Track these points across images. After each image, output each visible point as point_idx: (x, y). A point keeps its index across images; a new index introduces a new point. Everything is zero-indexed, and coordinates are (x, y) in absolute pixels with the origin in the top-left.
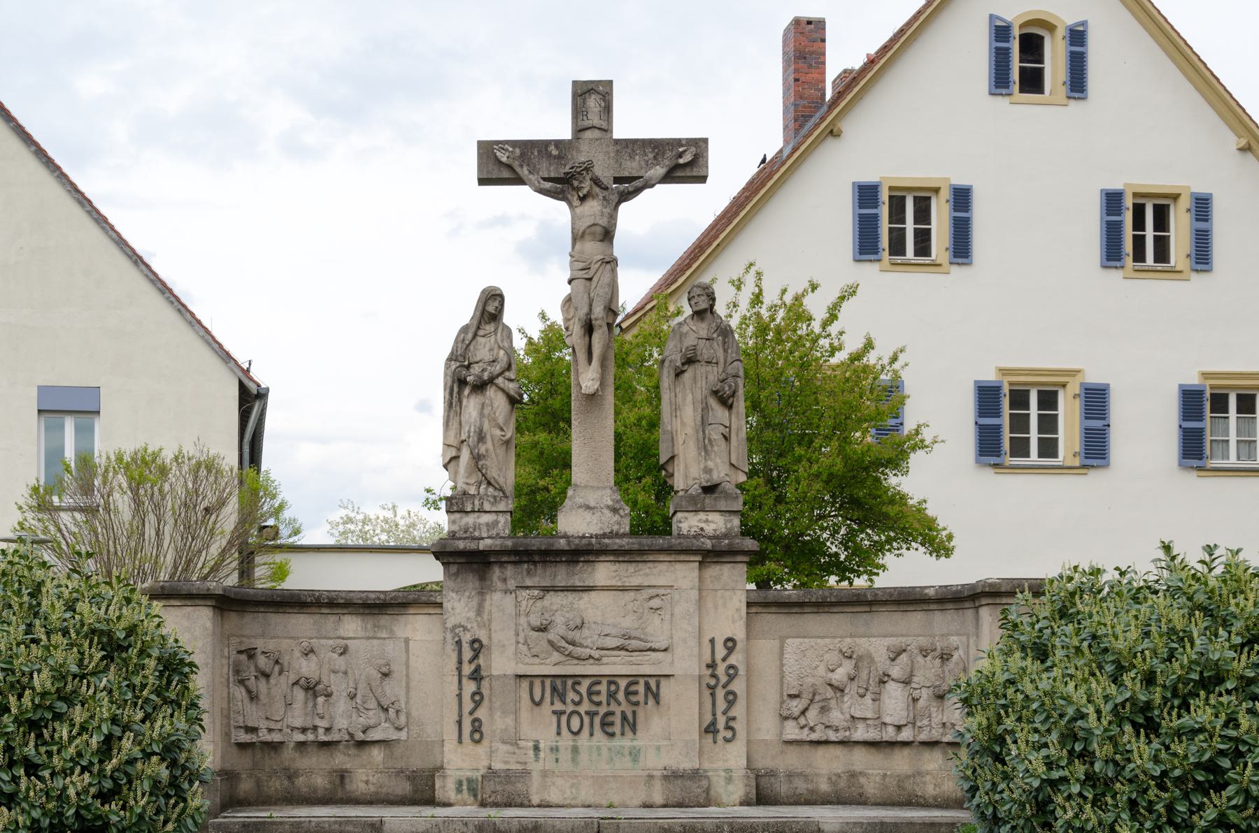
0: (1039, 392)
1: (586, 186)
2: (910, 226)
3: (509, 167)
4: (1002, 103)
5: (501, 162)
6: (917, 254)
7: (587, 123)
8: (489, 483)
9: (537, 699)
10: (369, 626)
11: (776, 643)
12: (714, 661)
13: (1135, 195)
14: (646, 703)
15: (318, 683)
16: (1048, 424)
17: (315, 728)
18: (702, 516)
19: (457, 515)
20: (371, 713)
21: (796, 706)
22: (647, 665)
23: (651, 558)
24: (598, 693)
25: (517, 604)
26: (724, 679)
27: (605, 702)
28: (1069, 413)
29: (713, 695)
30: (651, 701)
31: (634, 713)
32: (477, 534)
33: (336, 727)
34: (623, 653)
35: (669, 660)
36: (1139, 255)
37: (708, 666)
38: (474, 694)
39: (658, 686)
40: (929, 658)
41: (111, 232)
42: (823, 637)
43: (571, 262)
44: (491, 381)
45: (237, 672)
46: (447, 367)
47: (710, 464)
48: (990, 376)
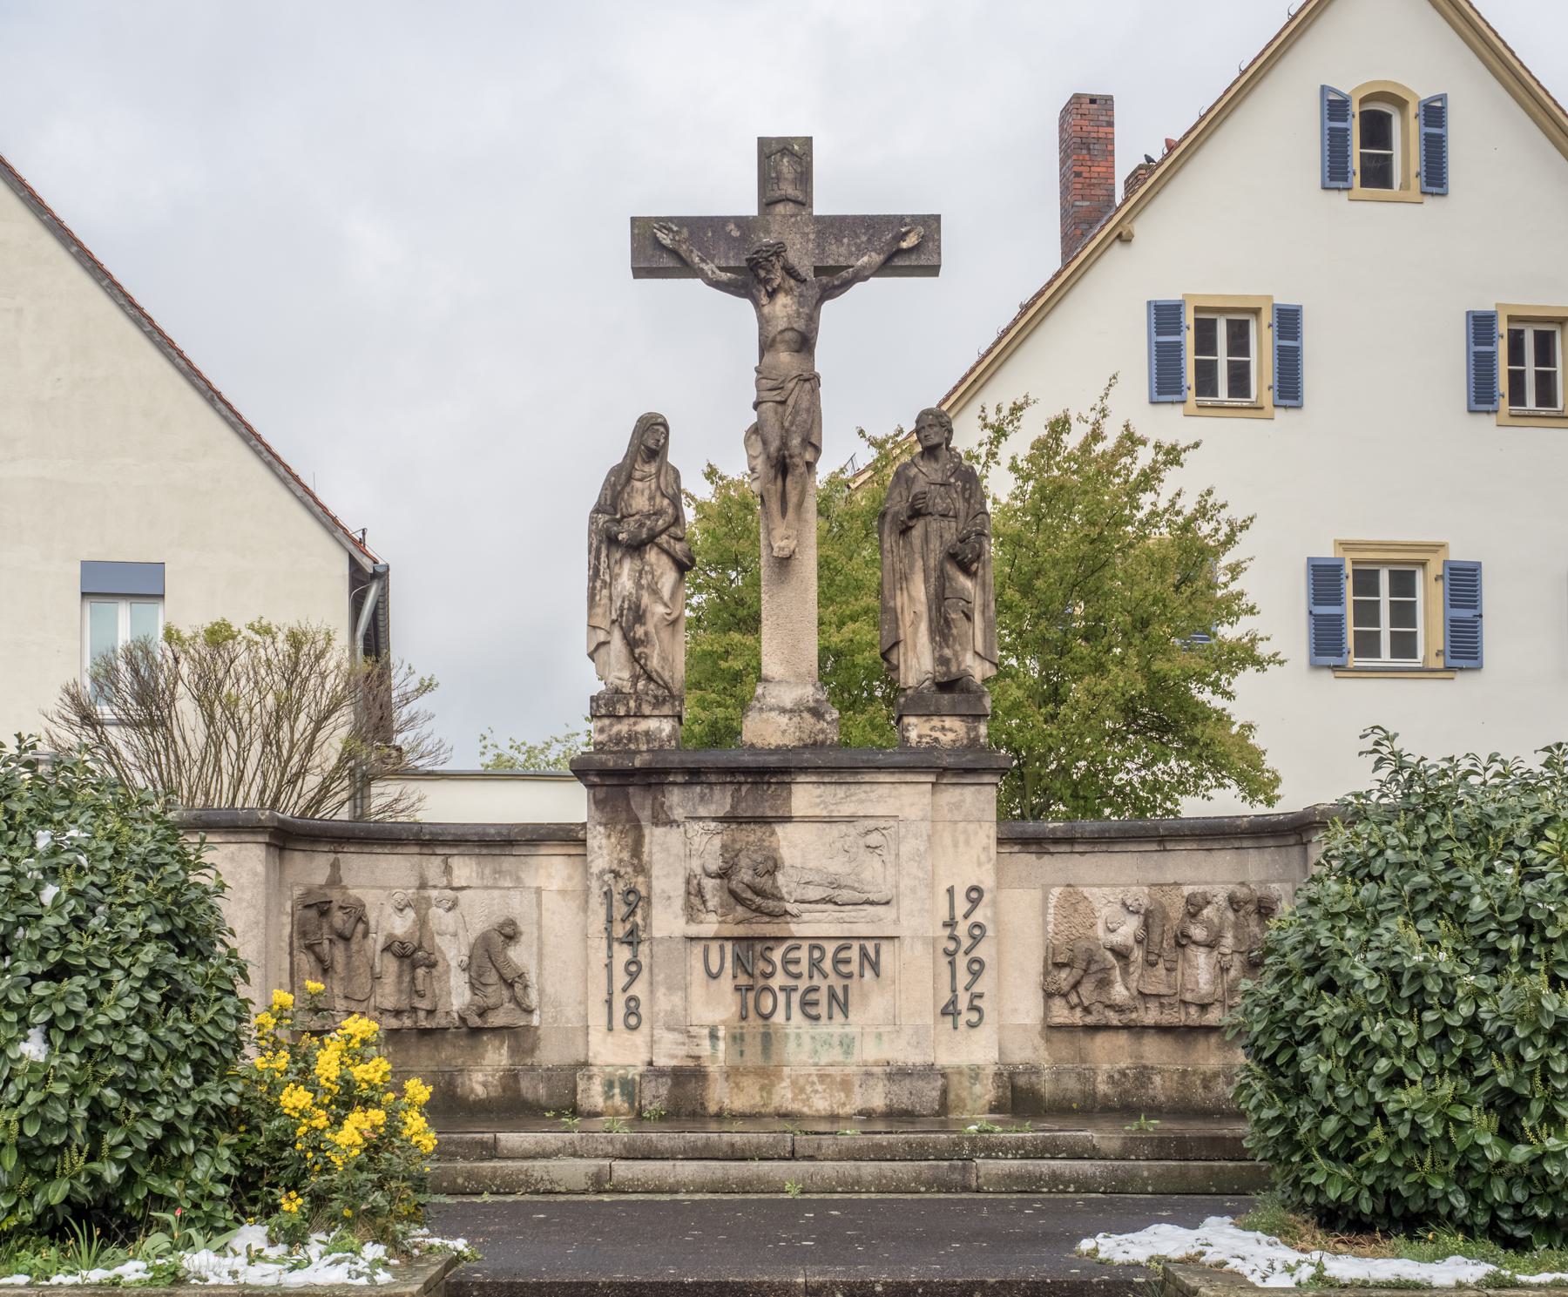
0: (1391, 572)
1: (778, 277)
2: (1222, 358)
3: (674, 253)
4: (1339, 199)
5: (664, 247)
6: (1233, 392)
7: (777, 194)
8: (650, 679)
9: (714, 970)
10: (487, 871)
11: (1037, 894)
12: (952, 918)
13: (1511, 319)
14: (862, 976)
15: (420, 947)
16: (1404, 614)
17: (414, 1010)
18: (936, 722)
19: (607, 721)
20: (490, 989)
21: (1064, 978)
22: (862, 923)
23: (867, 778)
24: (797, 962)
25: (687, 841)
26: (966, 942)
27: (806, 974)
28: (1429, 598)
29: (952, 964)
30: (868, 973)
31: (846, 988)
32: (632, 746)
33: (441, 1009)
34: (830, 907)
35: (894, 916)
36: (1517, 396)
37: (946, 925)
38: (630, 963)
39: (877, 952)
40: (1242, 913)
41: (179, 360)
42: (1100, 886)
43: (758, 380)
44: (652, 539)
45: (304, 934)
46: (592, 521)
47: (947, 652)
48: (1327, 552)
